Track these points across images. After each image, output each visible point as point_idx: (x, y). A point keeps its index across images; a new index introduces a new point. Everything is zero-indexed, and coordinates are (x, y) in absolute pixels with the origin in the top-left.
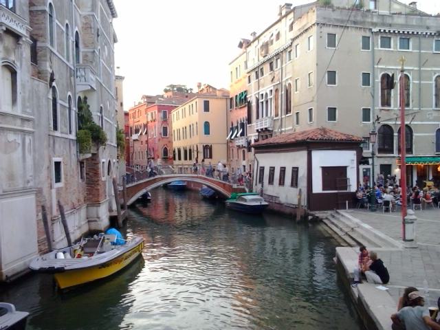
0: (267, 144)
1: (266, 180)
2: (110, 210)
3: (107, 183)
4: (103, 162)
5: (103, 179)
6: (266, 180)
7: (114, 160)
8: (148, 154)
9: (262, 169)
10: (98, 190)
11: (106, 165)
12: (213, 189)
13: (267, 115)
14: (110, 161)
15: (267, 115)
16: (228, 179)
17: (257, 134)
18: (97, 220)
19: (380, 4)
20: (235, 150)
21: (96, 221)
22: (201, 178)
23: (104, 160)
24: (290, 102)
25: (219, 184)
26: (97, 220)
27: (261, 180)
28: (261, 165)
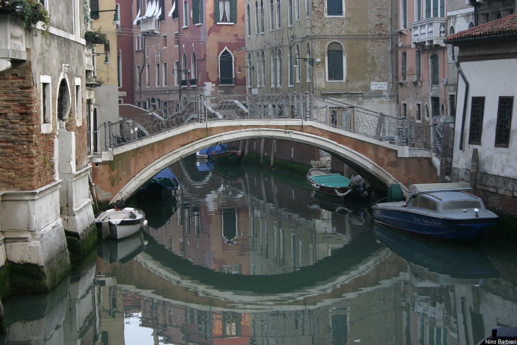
0: (261, 295)
1: (489, 133)
2: (66, 208)
3: (56, 141)
4: (45, 85)
5: (45, 129)
6: (489, 133)
7: (78, 81)
8: (179, 71)
9: (479, 103)
10: (29, 156)
11: (53, 93)
12: (356, 168)
13: (436, 15)
14: (63, 83)
15: (436, 15)
16: (201, 328)
17: (472, 9)
18: (28, 235)
19: (460, 333)
20: (411, 55)
21: (25, 240)
22: (313, 130)
23: (46, 79)
24: (16, 242)
25: (211, 302)
26: (28, 235)
27: (476, 135)
28: (474, 93)
